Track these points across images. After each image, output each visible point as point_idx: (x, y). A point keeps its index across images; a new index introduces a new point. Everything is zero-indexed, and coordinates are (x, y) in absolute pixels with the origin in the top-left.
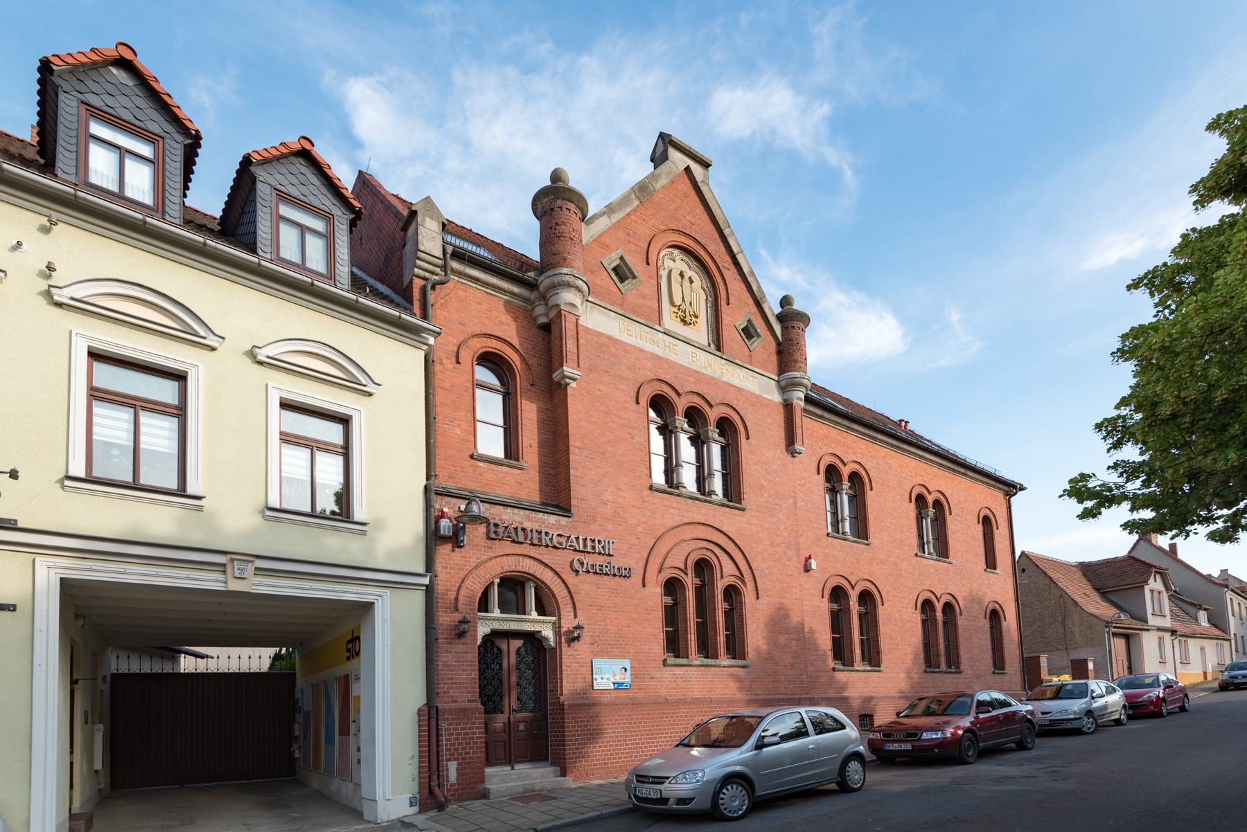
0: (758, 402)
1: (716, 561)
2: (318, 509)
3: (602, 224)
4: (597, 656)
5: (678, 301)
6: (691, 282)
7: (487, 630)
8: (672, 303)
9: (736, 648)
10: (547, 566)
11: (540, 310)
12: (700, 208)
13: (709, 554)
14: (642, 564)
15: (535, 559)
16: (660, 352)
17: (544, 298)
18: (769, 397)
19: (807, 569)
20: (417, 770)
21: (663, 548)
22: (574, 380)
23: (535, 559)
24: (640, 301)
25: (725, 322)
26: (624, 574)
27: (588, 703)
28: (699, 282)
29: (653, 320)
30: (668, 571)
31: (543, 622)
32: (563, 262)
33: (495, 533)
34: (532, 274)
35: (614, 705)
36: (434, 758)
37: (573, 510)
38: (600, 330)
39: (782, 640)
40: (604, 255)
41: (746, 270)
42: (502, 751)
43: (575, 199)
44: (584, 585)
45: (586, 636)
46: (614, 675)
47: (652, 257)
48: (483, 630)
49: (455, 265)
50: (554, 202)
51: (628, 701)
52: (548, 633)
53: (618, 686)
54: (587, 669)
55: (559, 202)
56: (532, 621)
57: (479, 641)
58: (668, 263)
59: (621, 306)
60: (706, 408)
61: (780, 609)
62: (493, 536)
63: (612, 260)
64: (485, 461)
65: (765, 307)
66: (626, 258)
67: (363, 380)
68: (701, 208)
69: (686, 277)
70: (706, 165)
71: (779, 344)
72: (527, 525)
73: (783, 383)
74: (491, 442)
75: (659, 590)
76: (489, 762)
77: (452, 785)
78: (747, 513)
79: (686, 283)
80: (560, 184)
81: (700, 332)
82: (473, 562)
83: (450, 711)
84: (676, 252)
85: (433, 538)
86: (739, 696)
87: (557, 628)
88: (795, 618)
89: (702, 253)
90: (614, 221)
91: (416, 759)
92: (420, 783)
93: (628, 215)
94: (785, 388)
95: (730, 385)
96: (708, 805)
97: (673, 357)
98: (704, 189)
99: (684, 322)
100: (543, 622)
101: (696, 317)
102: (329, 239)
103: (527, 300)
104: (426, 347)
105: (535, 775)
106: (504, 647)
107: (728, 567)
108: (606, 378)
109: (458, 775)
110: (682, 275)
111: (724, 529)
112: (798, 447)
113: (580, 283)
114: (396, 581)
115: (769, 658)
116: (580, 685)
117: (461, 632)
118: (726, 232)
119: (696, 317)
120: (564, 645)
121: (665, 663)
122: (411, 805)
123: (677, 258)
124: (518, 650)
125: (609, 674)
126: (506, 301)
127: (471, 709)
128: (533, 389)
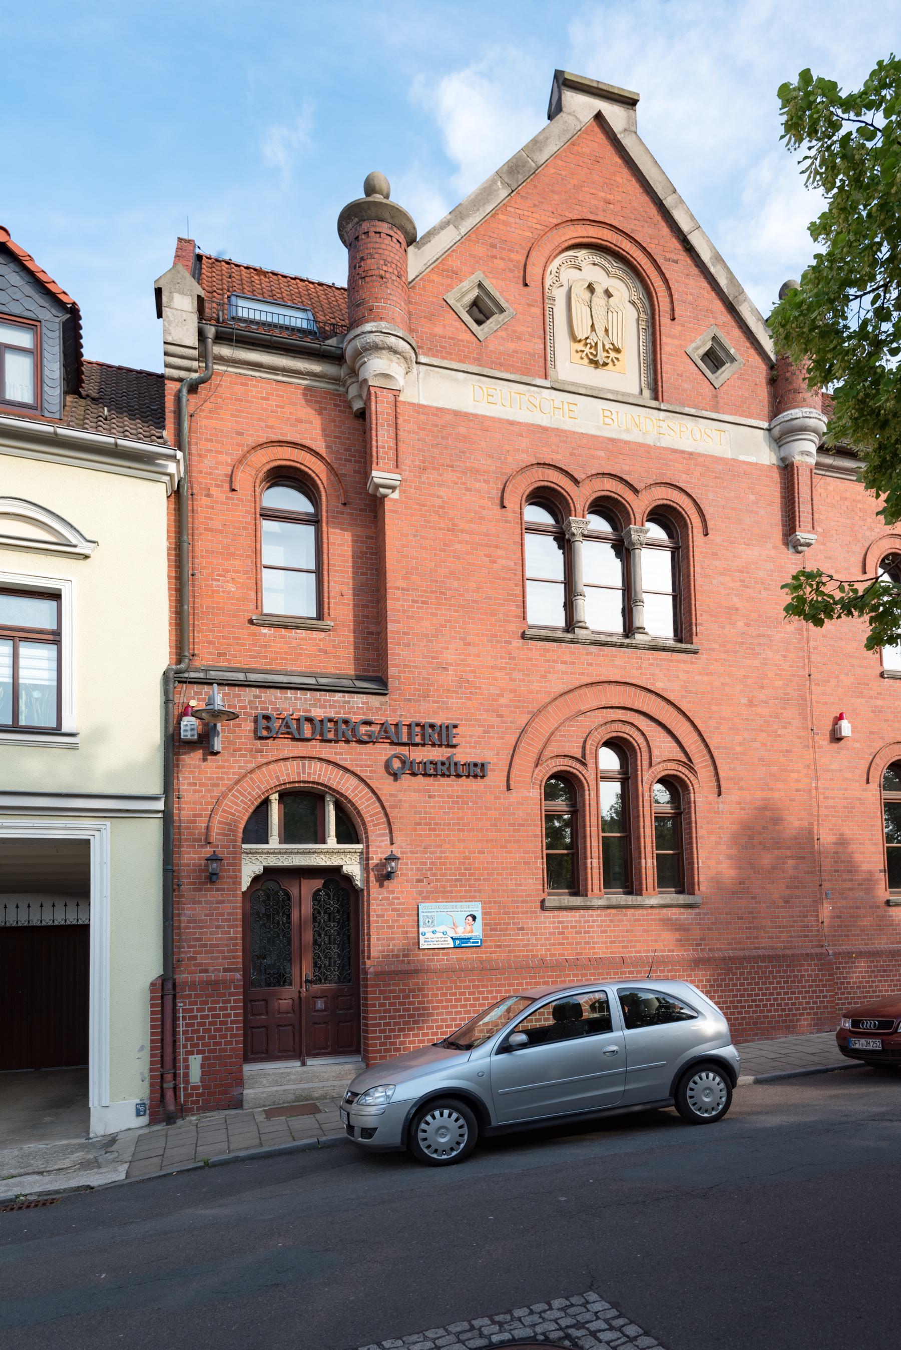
0: (731, 470)
1: (641, 740)
2: (23, 722)
3: (447, 239)
4: (426, 899)
5: (582, 331)
6: (608, 294)
7: (258, 869)
8: (574, 338)
9: (677, 873)
10: (346, 770)
11: (353, 391)
12: (624, 176)
13: (628, 729)
14: (506, 755)
15: (329, 762)
16: (543, 420)
17: (354, 372)
18: (752, 459)
19: (836, 737)
20: (148, 1066)
21: (544, 726)
22: (393, 488)
23: (329, 762)
24: (511, 346)
25: (667, 349)
26: (477, 770)
27: (409, 968)
28: (623, 291)
29: (537, 368)
30: (552, 763)
31: (344, 852)
32: (372, 314)
33: (266, 728)
34: (333, 341)
35: (450, 971)
36: (169, 1050)
37: (392, 683)
38: (440, 404)
39: (766, 860)
40: (449, 288)
41: (706, 256)
42: (265, 1039)
43: (387, 215)
44: (410, 793)
45: (405, 870)
46: (454, 927)
47: (534, 272)
48: (250, 869)
49: (225, 351)
50: (365, 221)
51: (470, 964)
52: (353, 868)
53: (461, 944)
54: (407, 921)
55: (365, 226)
56: (331, 852)
57: (245, 884)
58: (569, 275)
59: (478, 361)
60: (628, 495)
61: (764, 808)
62: (265, 733)
63: (463, 293)
64: (271, 626)
65: (745, 311)
66: (487, 284)
67: (73, 538)
68: (625, 172)
69: (599, 290)
70: (630, 102)
71: (772, 367)
72: (318, 713)
73: (776, 431)
74: (287, 594)
75: (535, 793)
76: (247, 1059)
77: (195, 1088)
78: (703, 657)
79: (599, 299)
80: (378, 198)
81: (627, 375)
82: (233, 774)
83: (193, 986)
84: (582, 254)
85: (175, 745)
86: (679, 953)
87: (365, 858)
88: (794, 822)
89: (627, 246)
90: (463, 231)
91: (147, 1052)
92: (152, 1085)
93: (494, 214)
94: (781, 438)
95: (674, 451)
96: (396, 1139)
97: (567, 424)
98: (628, 142)
99: (594, 363)
100: (344, 852)
101: (618, 351)
102: (36, 354)
103: (336, 380)
104: (166, 479)
105: (326, 1074)
106: (294, 892)
107: (663, 747)
108: (449, 476)
109: (203, 1074)
110: (591, 288)
111: (659, 686)
112: (802, 535)
113: (392, 341)
114: (120, 807)
115: (740, 889)
116: (397, 944)
117: (213, 873)
118: (668, 202)
119: (618, 351)
120: (373, 882)
121: (543, 906)
122: (138, 1114)
123: (583, 264)
124: (316, 894)
125: (444, 925)
126: (307, 389)
127: (224, 982)
128: (347, 510)
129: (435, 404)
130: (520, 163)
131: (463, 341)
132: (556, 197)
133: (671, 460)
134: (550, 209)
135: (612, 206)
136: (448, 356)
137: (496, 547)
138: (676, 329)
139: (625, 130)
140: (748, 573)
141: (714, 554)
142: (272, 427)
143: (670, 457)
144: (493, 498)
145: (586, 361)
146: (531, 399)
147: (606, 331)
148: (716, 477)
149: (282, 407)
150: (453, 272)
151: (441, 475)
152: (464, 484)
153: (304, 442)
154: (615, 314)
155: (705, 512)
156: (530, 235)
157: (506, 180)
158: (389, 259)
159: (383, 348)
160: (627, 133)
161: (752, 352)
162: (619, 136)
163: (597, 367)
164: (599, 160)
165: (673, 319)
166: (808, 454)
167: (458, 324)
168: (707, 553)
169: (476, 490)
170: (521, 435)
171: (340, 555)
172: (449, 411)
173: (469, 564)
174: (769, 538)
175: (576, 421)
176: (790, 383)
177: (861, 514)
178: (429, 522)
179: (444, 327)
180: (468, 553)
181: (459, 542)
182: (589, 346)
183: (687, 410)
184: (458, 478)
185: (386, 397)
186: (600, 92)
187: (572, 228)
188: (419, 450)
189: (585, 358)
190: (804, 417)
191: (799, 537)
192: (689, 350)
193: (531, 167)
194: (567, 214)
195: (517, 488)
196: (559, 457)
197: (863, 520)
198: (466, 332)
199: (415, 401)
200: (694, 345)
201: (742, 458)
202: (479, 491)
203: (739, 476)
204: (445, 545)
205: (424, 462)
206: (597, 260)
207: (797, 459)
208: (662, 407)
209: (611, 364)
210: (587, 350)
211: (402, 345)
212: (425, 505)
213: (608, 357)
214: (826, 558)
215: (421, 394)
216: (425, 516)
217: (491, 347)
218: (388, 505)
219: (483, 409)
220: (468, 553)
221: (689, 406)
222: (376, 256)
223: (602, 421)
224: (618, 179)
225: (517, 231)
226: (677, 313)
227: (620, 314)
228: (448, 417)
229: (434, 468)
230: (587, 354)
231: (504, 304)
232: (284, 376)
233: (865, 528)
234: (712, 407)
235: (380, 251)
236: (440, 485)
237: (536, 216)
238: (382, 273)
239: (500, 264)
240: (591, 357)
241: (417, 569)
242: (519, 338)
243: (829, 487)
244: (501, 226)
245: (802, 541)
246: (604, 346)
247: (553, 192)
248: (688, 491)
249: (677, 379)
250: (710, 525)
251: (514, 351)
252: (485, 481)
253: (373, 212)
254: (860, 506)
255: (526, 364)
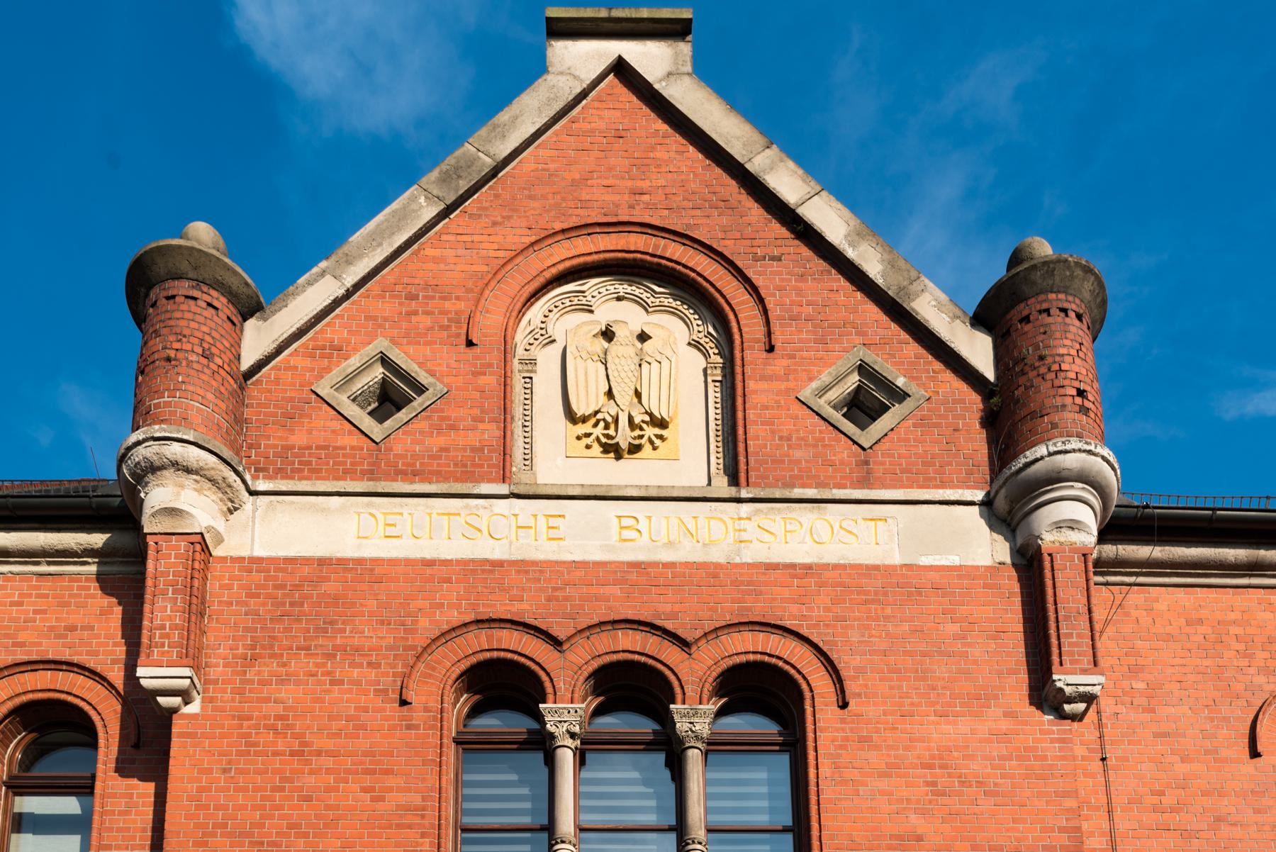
8: (571, 417)
24: (438, 441)
43: (184, 266)
60: (670, 654)
66: (397, 356)
89: (675, 251)
94: (1010, 508)
99: (613, 449)
101: (662, 424)
113: (175, 450)
129: (282, 553)
130: (462, 163)
131: (344, 448)
132: (533, 204)
133: (766, 584)
134: (524, 224)
135: (646, 198)
136: (316, 473)
137: (388, 772)
138: (778, 364)
139: (669, 74)
140: (942, 767)
141: (862, 740)
142: (22, 645)
143: (762, 578)
144: (385, 691)
145: (597, 449)
146: (472, 520)
147: (638, 394)
148: (866, 602)
149: (44, 612)
150: (333, 348)
151: (284, 665)
152: (328, 673)
153: (75, 659)
154: (655, 365)
155: (840, 666)
156: (485, 268)
157: (435, 192)
158: (186, 332)
159: (162, 468)
160: (672, 78)
161: (948, 376)
162: (656, 86)
163: (619, 457)
164: (623, 134)
165: (771, 349)
166: (1073, 525)
167: (338, 424)
168: (846, 739)
169: (351, 682)
170: (449, 581)
171: (119, 830)
172: (307, 561)
173: (328, 807)
174: (996, 697)
175: (562, 543)
176: (1024, 405)
177: (1241, 647)
178: (256, 744)
179: (309, 432)
180: (328, 789)
181: (312, 772)
182: (602, 424)
183: (798, 492)
184: (317, 665)
185: (177, 548)
186: (618, 27)
187: (567, 243)
188: (246, 629)
189: (596, 445)
190: (1050, 454)
191: (1059, 684)
192: (806, 393)
193: (484, 164)
194: (1110, 631)
195: (434, 669)
196: (525, 606)
197: (1245, 656)
198: (350, 433)
199: (245, 553)
200: (814, 385)
201: (925, 561)
202: (358, 683)
203: (920, 594)
204: (282, 780)
205: (253, 647)
206: (623, 288)
207: (1049, 539)
208: (744, 494)
209: (648, 447)
210: (599, 430)
211: (193, 455)
212: (250, 718)
213: (641, 437)
214: (1156, 735)
215: (257, 540)
216: (249, 735)
217: (398, 449)
218: (177, 727)
219: (377, 548)
220: (328, 789)
221: (803, 486)
222: (164, 331)
223: (617, 538)
224: (660, 154)
225: (458, 267)
226: (778, 339)
227: (665, 363)
228: (306, 570)
229: (272, 656)
230: (598, 439)
231: (424, 378)
232: (49, 563)
233: (1252, 671)
234: (864, 480)
235: (172, 323)
236: (281, 682)
237: (499, 238)
238: (172, 354)
239: (423, 321)
240: (604, 440)
241: (225, 825)
242: (452, 427)
243: (1155, 605)
244: (431, 265)
245: (1068, 690)
246: (631, 419)
247: (530, 197)
248: (804, 631)
249: (778, 447)
250: (850, 687)
251: (442, 449)
252: (370, 664)
253: (161, 268)
254: (1235, 630)
255: (465, 466)
